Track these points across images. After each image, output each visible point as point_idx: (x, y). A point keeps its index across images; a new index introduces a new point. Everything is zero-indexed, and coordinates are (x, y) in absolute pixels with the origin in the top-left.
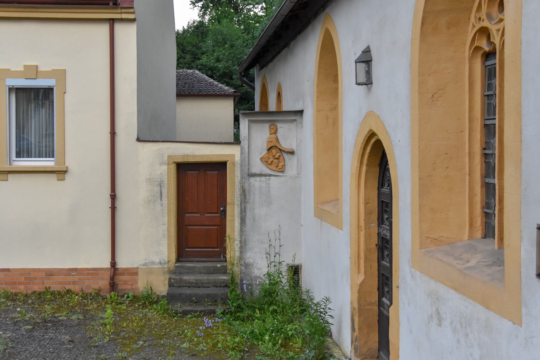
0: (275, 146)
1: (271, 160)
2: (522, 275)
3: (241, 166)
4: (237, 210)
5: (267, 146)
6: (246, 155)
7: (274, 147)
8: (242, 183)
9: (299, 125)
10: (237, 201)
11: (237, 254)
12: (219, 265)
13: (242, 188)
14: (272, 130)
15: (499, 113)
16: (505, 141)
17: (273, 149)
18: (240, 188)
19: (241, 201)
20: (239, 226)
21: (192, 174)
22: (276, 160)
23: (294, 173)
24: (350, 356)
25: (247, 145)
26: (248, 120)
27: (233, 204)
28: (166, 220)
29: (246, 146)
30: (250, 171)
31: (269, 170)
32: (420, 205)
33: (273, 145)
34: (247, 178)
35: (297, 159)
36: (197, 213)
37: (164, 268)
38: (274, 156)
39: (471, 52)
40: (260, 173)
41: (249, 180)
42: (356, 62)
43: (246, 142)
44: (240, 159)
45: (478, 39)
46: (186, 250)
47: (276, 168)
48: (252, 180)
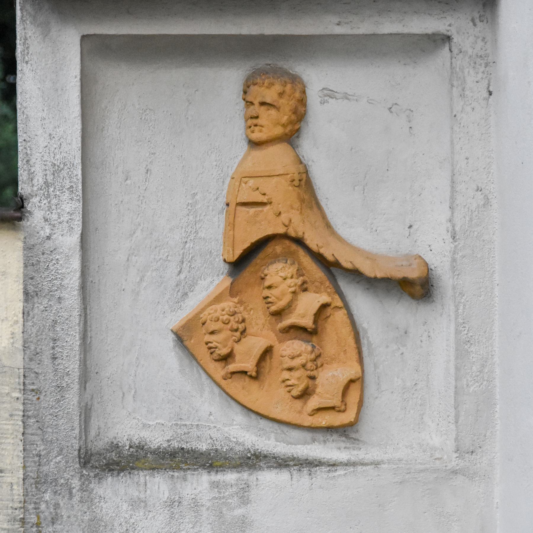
0: (285, 236)
5: (225, 234)
6: (67, 303)
7: (278, 248)
8: (38, 525)
9: (470, 80)
16: (278, 418)
17: (276, 258)
23: (436, 441)
25: (71, 229)
30: (93, 433)
33: (270, 231)
34: (76, 483)
35: (457, 332)
38: (278, 314)
40: (175, 444)
43: (67, 207)
44: (19, 336)
47: (298, 404)
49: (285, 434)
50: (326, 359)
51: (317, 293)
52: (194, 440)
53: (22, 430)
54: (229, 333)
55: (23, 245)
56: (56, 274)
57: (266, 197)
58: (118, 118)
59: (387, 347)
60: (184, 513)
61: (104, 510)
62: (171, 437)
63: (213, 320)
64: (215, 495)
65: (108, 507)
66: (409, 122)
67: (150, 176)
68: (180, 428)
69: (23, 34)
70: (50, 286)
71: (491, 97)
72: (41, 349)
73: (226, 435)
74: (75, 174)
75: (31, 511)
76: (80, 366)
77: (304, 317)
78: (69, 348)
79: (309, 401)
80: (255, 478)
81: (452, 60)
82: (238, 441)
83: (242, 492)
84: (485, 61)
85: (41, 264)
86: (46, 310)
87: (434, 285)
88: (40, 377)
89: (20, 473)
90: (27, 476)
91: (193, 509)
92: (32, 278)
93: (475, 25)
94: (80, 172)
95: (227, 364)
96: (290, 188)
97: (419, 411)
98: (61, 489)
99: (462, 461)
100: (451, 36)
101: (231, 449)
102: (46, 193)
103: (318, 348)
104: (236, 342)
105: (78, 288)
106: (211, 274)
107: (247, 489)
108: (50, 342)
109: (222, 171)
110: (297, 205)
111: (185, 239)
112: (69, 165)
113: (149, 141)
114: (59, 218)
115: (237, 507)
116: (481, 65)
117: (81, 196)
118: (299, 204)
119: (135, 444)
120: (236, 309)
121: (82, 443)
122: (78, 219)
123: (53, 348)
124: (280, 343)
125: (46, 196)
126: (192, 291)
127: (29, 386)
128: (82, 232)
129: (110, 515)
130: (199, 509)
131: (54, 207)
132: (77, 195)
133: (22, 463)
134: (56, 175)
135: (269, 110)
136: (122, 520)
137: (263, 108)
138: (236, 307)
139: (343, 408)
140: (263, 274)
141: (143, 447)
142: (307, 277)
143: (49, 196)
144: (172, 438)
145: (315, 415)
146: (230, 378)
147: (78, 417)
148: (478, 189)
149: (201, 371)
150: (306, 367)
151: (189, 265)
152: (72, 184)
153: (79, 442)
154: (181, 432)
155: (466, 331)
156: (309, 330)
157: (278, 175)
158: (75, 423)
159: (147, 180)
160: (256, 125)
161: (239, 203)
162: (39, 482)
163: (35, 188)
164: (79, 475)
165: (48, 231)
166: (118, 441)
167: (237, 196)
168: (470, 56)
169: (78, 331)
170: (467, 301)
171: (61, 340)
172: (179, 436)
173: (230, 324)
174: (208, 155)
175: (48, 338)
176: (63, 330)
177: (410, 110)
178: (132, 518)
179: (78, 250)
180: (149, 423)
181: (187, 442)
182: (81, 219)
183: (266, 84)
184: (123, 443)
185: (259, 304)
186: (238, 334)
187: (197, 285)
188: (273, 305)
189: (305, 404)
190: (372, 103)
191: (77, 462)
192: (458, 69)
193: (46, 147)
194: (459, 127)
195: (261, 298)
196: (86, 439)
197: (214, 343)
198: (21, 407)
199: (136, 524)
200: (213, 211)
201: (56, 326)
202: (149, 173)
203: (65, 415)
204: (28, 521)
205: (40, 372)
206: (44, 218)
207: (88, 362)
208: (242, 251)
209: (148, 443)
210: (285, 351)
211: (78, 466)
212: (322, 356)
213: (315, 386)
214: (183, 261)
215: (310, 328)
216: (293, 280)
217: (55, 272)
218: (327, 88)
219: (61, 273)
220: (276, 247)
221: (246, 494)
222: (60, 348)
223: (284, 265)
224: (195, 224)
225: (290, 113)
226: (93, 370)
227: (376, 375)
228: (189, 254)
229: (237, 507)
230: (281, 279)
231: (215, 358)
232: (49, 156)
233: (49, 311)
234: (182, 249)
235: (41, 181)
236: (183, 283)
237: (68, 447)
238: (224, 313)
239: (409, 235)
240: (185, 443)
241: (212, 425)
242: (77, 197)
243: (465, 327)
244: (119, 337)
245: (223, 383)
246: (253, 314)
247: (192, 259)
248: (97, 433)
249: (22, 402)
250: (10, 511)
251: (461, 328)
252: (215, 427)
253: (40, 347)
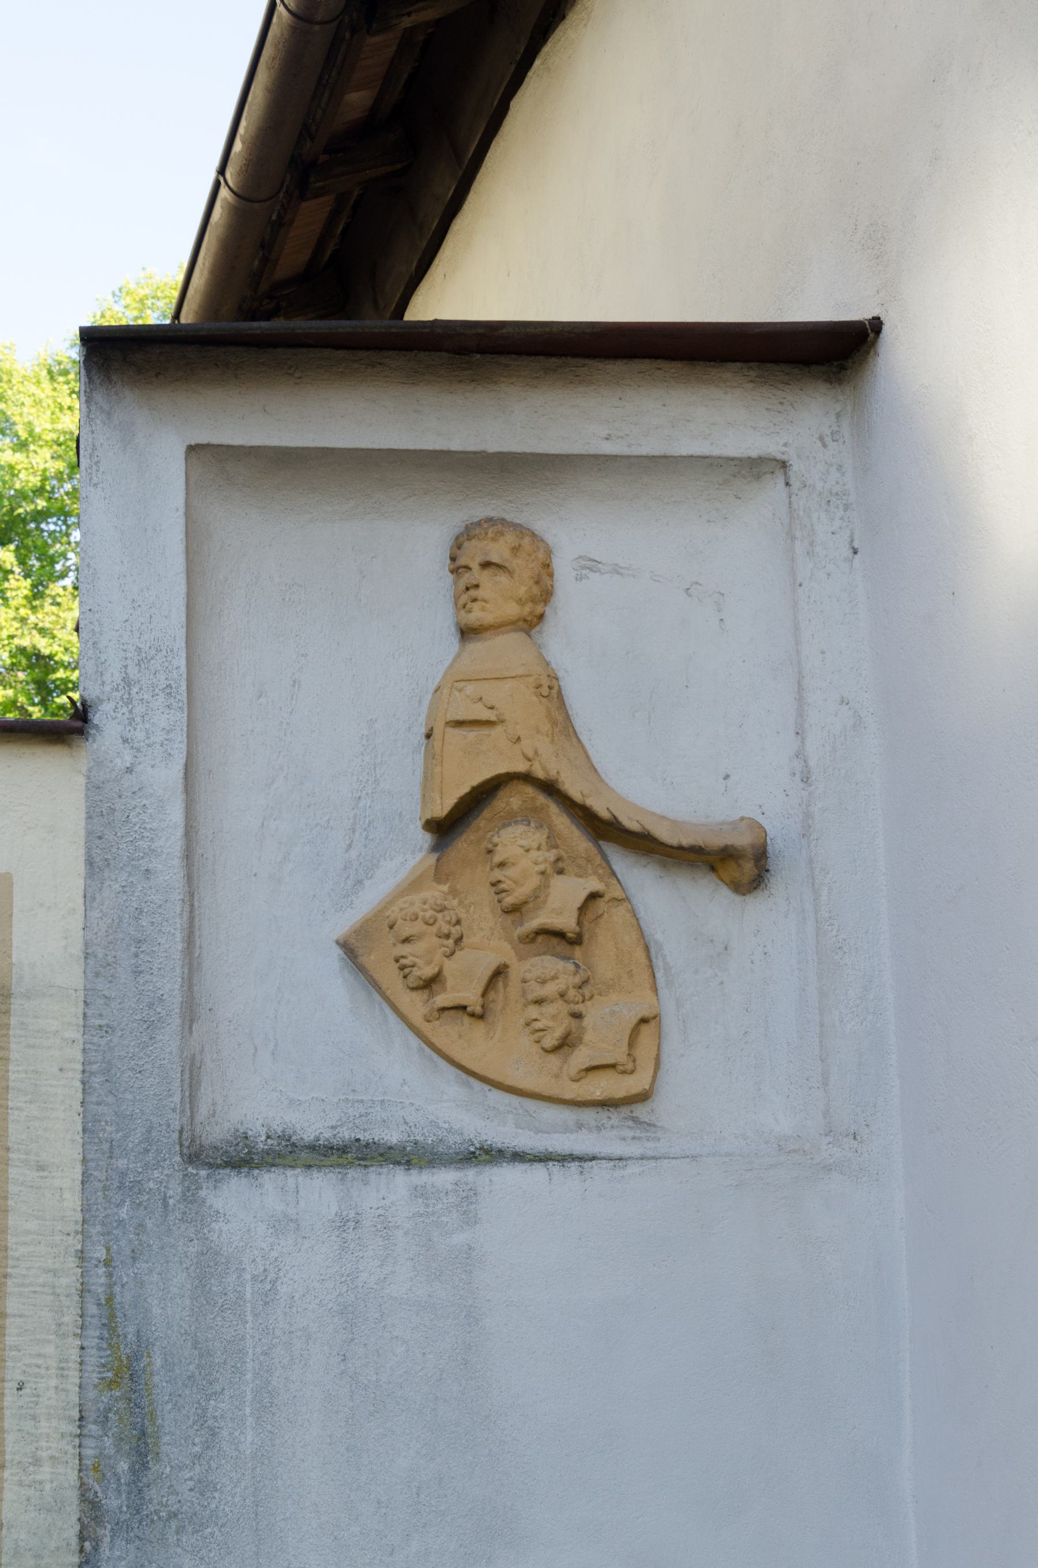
0: (526, 778)
8: (107, 1263)
13: (110, 1326)
14: (484, 578)
17: (510, 819)
18: (71, 1317)
24: (639, 826)
26: (180, 452)
30: (203, 1110)
33: (502, 769)
38: (515, 910)
41: (190, 1196)
47: (554, 1060)
49: (531, 1116)
50: (599, 986)
51: (581, 876)
52: (377, 1125)
53: (80, 1096)
54: (435, 940)
55: (85, 782)
56: (142, 830)
57: (495, 712)
58: (246, 598)
59: (696, 971)
60: (365, 1241)
61: (224, 1235)
62: (337, 1121)
63: (408, 918)
64: (417, 1210)
65: (231, 1231)
66: (719, 611)
67: (298, 691)
68: (352, 1106)
69: (90, 440)
70: (131, 851)
71: (857, 557)
72: (115, 957)
73: (431, 1118)
74: (175, 666)
75: (95, 1238)
76: (182, 986)
77: (561, 913)
78: (163, 955)
79: (573, 1056)
80: (487, 1180)
81: (792, 499)
82: (452, 1128)
83: (466, 1203)
84: (844, 502)
85: (116, 813)
86: (125, 892)
87: (771, 868)
88: (113, 1005)
89: (75, 1171)
90: (88, 1177)
91: (381, 1233)
92: (100, 838)
93: (825, 445)
94: (183, 663)
95: (432, 995)
96: (534, 698)
97: (753, 1077)
98: (149, 1199)
99: (839, 1150)
100: (788, 462)
101: (440, 1140)
102: (126, 696)
103: (584, 969)
104: (447, 957)
105: (179, 855)
106: (402, 850)
107: (474, 1199)
108: (131, 945)
109: (417, 684)
110: (546, 727)
111: (357, 793)
112: (164, 651)
113: (297, 636)
114: (148, 738)
115: (457, 1229)
116: (837, 507)
117: (185, 702)
118: (549, 725)
119: (277, 1133)
120: (445, 903)
121: (185, 1120)
122: (179, 739)
123: (136, 956)
124: (520, 960)
125: (125, 700)
126: (371, 878)
127: (93, 1021)
128: (186, 761)
129: (236, 1243)
130: (390, 1233)
131: (138, 719)
132: (179, 700)
133: (79, 1154)
134: (143, 666)
135: (496, 575)
136: (256, 1253)
137: (487, 573)
138: (446, 900)
139: (630, 1066)
140: (491, 843)
141: (290, 1137)
142: (563, 850)
143: (130, 700)
144: (338, 1123)
145: (583, 1081)
146: (438, 1019)
147: (179, 1075)
148: (844, 701)
149: (388, 1011)
150: (566, 998)
151: (364, 836)
152: (170, 682)
153: (180, 1117)
154: (355, 1113)
155: (835, 931)
156: (570, 935)
157: (512, 677)
158: (172, 1084)
159: (294, 697)
160: (474, 600)
161: (451, 721)
162: (109, 1186)
163: (107, 688)
164: (180, 1175)
165: (128, 759)
166: (247, 1129)
167: (447, 710)
168: (820, 494)
169: (179, 926)
170: (834, 882)
171: (149, 942)
172: (351, 1119)
173: (437, 925)
174: (394, 658)
175: (127, 939)
176: (152, 926)
177: (720, 593)
178: (273, 1249)
179: (180, 790)
180: (300, 1099)
181: (365, 1130)
182: (186, 740)
183: (490, 535)
184: (255, 1131)
185: (486, 894)
186: (450, 942)
187: (378, 868)
188: (508, 896)
189: (565, 1062)
190: (658, 581)
191: (176, 1152)
192: (801, 513)
193: (127, 621)
194: (808, 603)
195: (488, 885)
196: (192, 1117)
197: (411, 958)
198: (80, 1057)
199: (280, 1259)
200: (403, 747)
201: (141, 917)
202: (297, 686)
203: (156, 1071)
204: (90, 1255)
205: (113, 996)
206: (122, 738)
207: (196, 988)
208: (456, 801)
209: (299, 1132)
210: (530, 972)
211: (178, 1158)
212: (592, 981)
213: (582, 1030)
214: (354, 828)
215: (572, 932)
216: (540, 853)
217: (140, 827)
218: (585, 556)
219: (151, 829)
220: (512, 799)
221: (472, 1207)
222: (148, 954)
223: (526, 828)
224: (375, 768)
225: (531, 583)
226: (203, 1003)
227: (680, 1017)
228: (365, 817)
229: (457, 1229)
230: (520, 851)
231: (411, 985)
232: (132, 637)
233: (130, 893)
234: (353, 809)
235: (118, 678)
236: (355, 866)
237: (160, 1125)
238: (426, 907)
239: (726, 790)
240: (362, 1132)
241: (407, 1102)
242: (178, 704)
243: (832, 925)
244: (248, 953)
245: (426, 1028)
246: (474, 912)
247: (369, 826)
248: (211, 1112)
249: (81, 1046)
250: (57, 1238)
251: (826, 927)
252: (412, 1104)
253: (113, 953)
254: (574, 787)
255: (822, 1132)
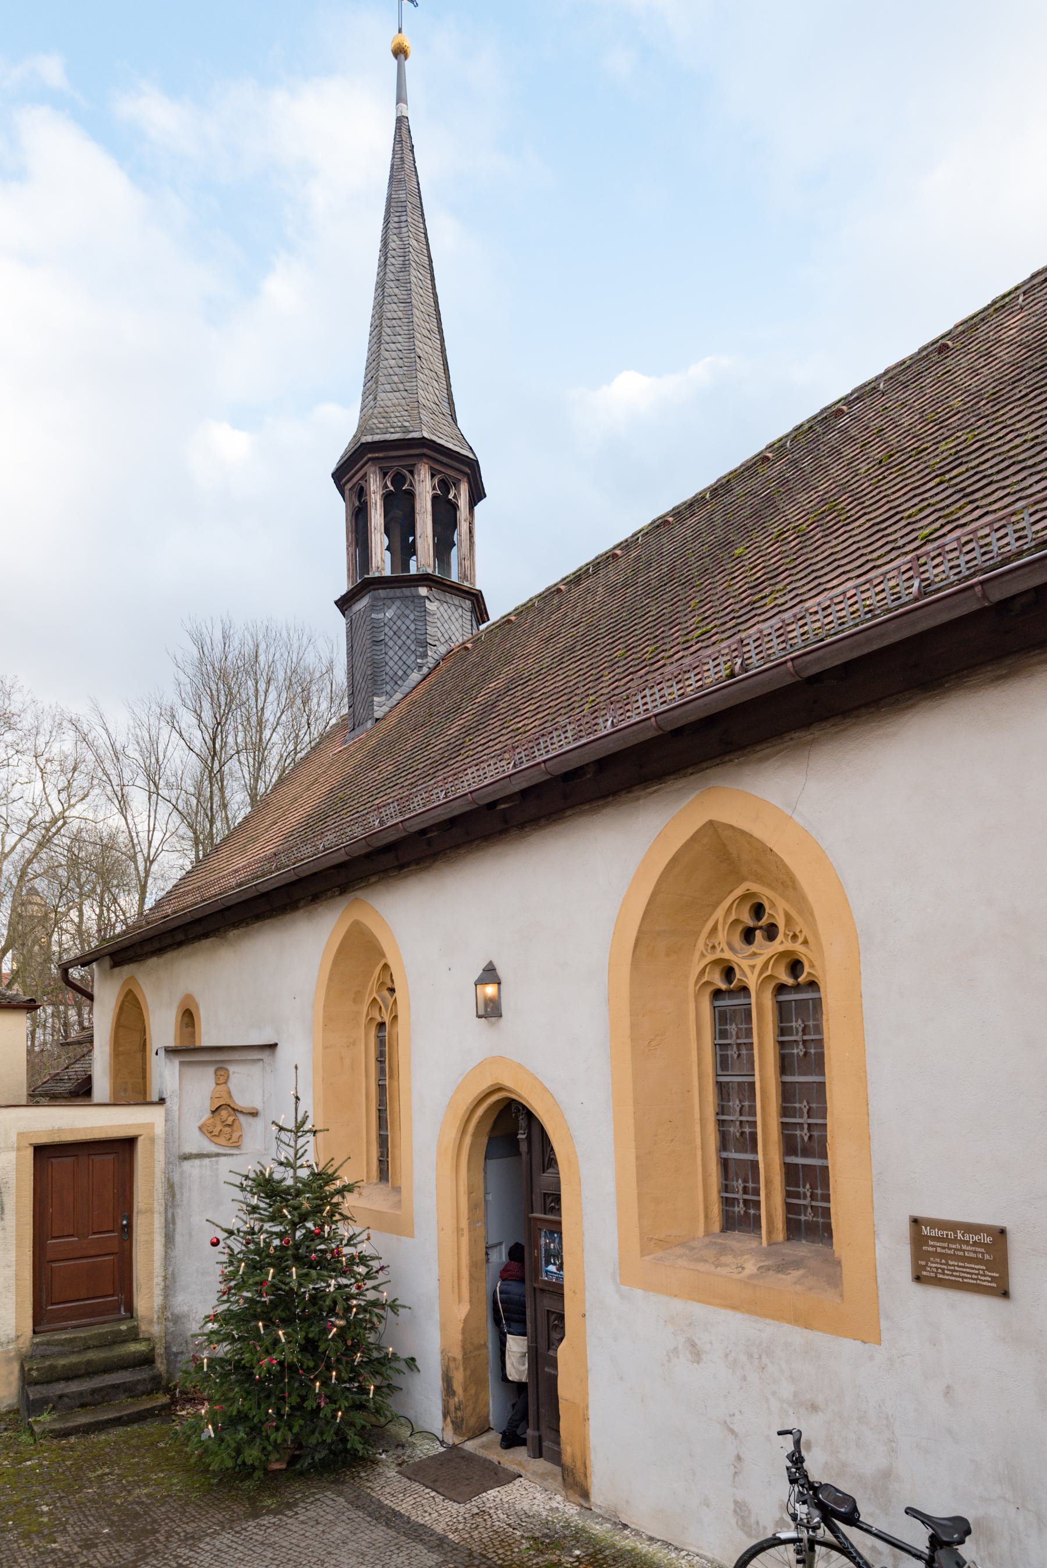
1: (218, 1128)
2: (879, 1279)
3: (167, 1142)
4: (158, 1222)
7: (223, 1107)
10: (158, 1206)
11: (158, 1300)
12: (123, 1327)
15: (760, 1071)
19: (166, 1205)
20: (163, 1249)
21: (61, 1164)
22: (227, 1129)
23: (258, 1147)
27: (150, 1211)
28: (12, 1256)
29: (176, 1108)
31: (213, 1145)
32: (639, 1194)
36: (72, 1236)
37: (9, 1351)
38: (223, 1122)
39: (697, 988)
42: (476, 985)
45: (709, 973)
46: (49, 1308)
48: (187, 1165)
124: (153, 1124)
254: (232, 1105)
255: (389, 1313)
